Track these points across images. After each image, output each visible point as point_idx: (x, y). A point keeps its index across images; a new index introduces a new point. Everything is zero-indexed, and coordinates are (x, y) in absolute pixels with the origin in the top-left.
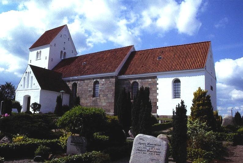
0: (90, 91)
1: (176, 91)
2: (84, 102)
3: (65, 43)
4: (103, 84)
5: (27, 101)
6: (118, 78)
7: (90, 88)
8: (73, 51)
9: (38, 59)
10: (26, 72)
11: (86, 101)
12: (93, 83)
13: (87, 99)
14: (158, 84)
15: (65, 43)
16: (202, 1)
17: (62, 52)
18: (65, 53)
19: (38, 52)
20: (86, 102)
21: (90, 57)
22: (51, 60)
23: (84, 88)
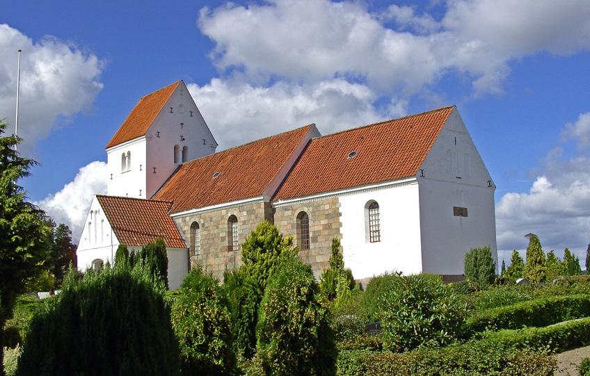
0: (223, 239)
1: (374, 222)
2: (213, 263)
3: (182, 124)
4: (244, 223)
5: (304, 147)
6: (271, 206)
7: (222, 232)
8: (204, 140)
9: (126, 170)
10: (92, 212)
11: (217, 261)
12: (226, 222)
13: (218, 257)
14: (340, 215)
15: (182, 124)
16: (2, 23)
17: (176, 148)
18: (185, 149)
19: (124, 154)
20: (217, 263)
21: (230, 157)
22: (151, 171)
23: (212, 232)
